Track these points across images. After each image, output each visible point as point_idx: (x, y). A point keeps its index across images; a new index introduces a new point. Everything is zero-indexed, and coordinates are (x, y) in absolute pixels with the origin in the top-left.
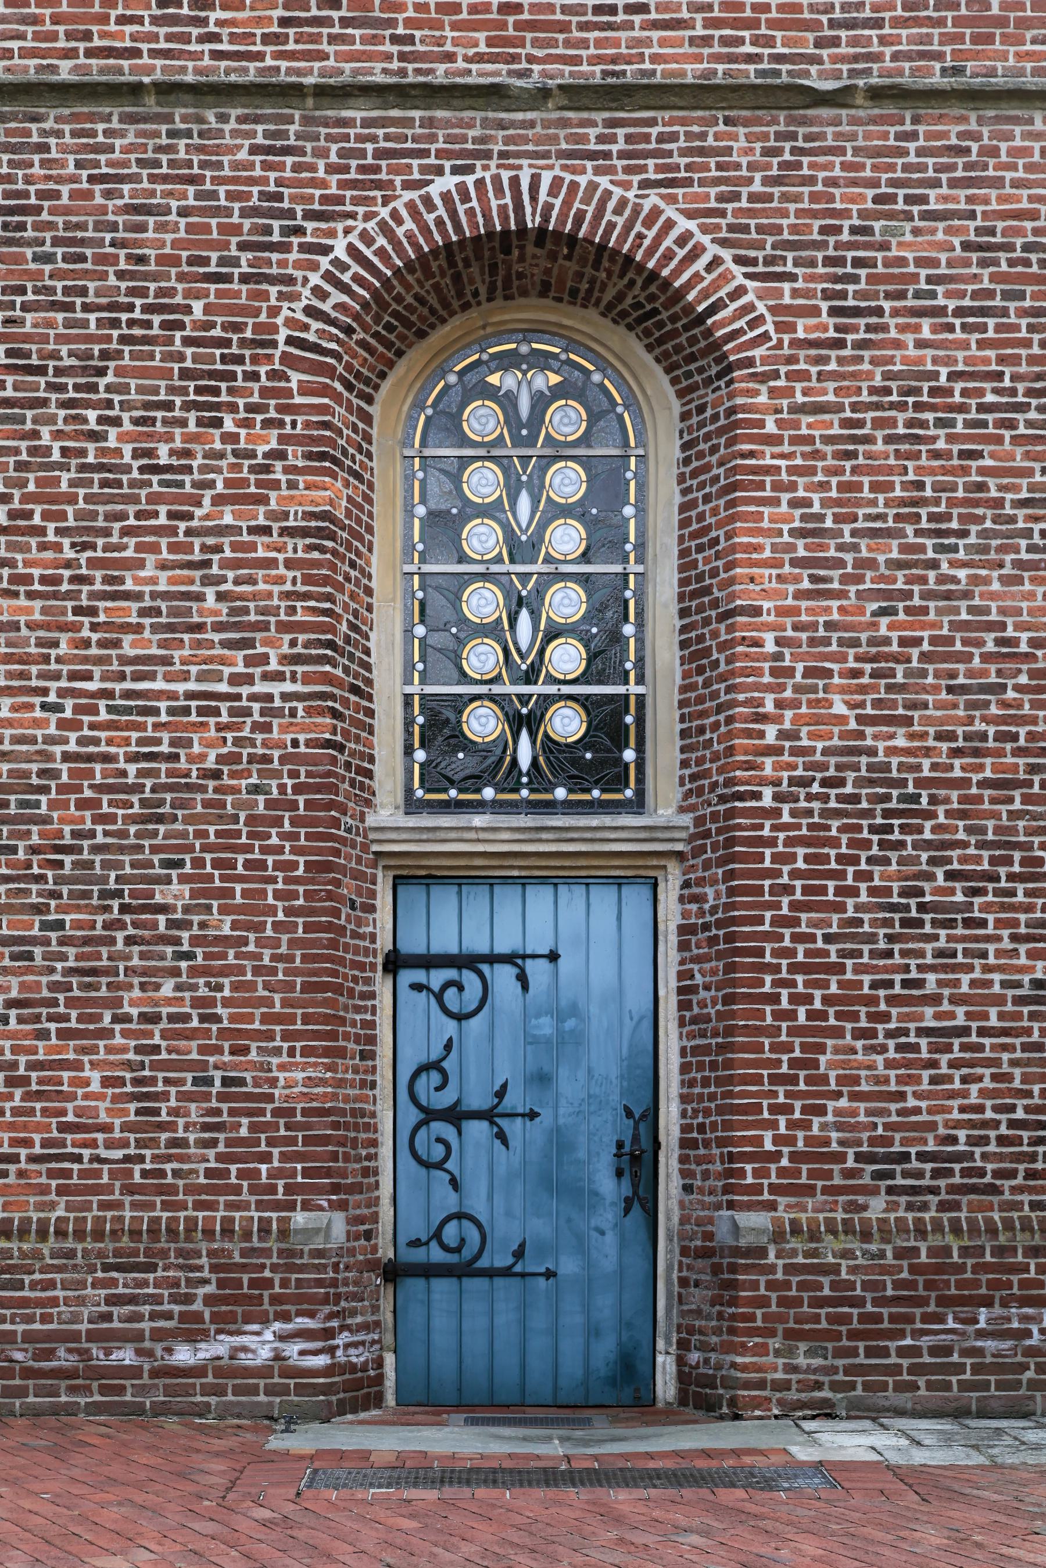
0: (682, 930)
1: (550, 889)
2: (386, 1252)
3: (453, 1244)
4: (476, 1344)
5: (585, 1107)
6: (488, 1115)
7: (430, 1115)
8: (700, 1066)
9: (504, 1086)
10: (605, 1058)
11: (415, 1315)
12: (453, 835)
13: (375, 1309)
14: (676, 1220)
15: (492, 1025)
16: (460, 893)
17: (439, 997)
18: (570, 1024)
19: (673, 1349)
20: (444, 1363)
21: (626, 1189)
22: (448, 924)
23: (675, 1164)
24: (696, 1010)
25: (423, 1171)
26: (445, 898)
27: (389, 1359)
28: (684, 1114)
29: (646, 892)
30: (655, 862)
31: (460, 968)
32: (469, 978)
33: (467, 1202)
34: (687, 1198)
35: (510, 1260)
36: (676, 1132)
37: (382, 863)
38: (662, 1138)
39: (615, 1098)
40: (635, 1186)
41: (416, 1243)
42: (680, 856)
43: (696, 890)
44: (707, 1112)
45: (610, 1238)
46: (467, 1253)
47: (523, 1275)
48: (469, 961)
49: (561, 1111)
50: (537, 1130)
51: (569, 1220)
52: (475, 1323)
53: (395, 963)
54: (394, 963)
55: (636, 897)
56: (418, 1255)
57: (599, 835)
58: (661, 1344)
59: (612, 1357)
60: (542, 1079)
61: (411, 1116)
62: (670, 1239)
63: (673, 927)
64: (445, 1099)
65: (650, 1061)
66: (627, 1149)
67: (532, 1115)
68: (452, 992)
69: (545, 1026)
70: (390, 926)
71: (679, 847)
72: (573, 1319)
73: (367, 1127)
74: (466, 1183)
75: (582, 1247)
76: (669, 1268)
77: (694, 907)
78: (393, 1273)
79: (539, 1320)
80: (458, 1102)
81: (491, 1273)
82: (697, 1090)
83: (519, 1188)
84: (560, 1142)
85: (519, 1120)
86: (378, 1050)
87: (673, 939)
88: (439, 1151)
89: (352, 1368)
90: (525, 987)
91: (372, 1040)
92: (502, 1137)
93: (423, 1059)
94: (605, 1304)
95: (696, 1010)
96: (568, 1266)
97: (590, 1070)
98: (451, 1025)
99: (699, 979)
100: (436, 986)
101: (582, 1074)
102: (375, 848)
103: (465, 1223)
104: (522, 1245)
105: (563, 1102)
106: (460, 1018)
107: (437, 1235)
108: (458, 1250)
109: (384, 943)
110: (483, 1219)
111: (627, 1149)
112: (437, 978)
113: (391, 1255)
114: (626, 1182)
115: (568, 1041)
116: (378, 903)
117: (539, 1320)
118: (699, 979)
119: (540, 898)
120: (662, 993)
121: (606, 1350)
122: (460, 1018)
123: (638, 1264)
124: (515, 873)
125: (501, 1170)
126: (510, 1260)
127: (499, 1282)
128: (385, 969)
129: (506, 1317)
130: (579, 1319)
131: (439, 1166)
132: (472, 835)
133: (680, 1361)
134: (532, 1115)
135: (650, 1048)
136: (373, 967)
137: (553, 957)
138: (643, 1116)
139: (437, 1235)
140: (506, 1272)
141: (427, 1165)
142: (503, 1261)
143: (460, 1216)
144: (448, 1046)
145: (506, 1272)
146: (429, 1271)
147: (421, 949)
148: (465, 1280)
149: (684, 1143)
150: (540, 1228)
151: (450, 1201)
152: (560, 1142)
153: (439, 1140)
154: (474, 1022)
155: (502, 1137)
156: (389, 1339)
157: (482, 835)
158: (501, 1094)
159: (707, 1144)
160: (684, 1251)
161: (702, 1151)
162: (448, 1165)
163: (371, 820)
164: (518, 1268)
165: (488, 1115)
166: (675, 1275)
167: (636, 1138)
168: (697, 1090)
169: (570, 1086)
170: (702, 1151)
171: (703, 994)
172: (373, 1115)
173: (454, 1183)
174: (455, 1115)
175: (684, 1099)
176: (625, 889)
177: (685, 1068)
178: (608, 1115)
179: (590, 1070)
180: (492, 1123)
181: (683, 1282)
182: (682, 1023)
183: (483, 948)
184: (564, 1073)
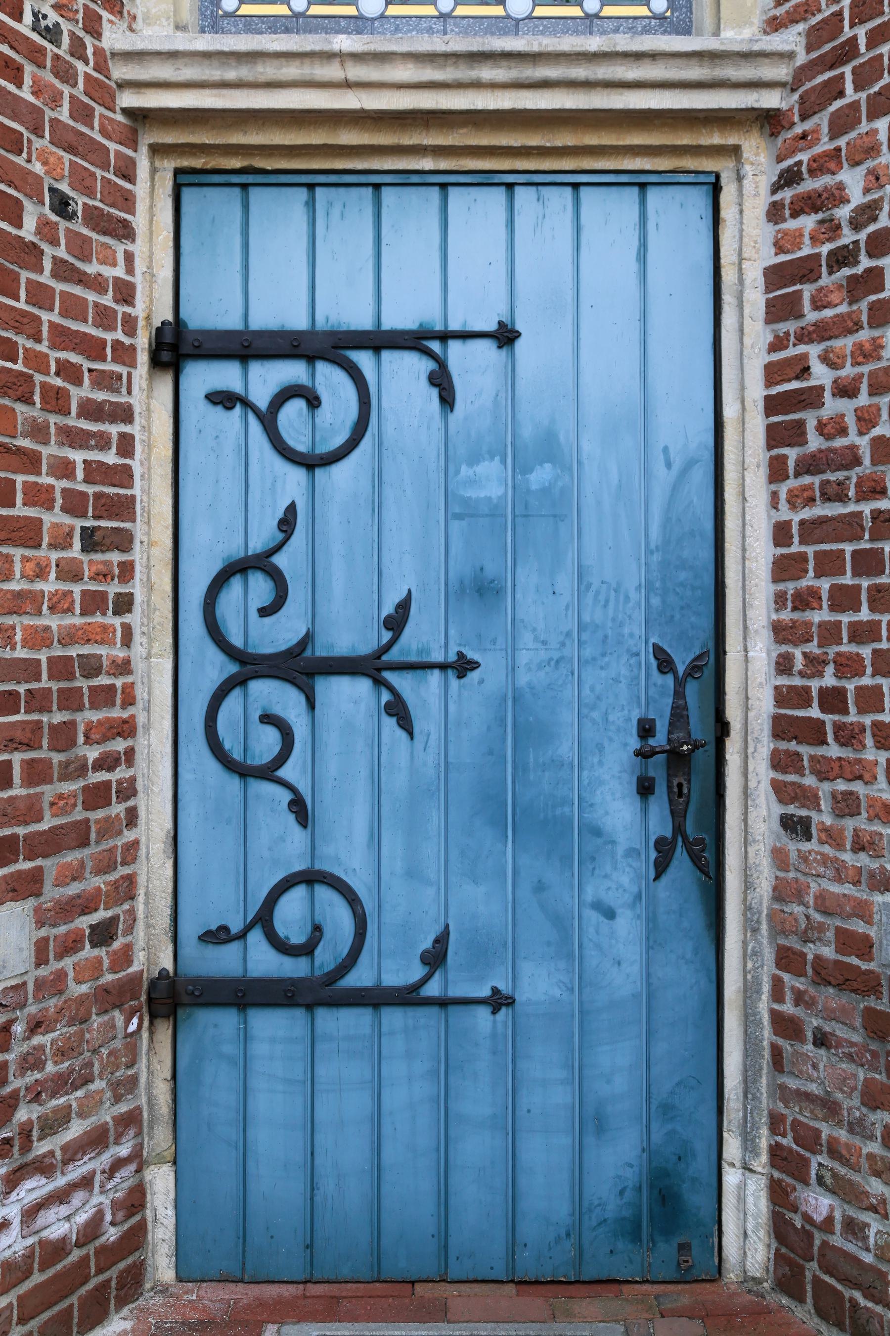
0: (775, 276)
1: (500, 194)
2: (151, 951)
3: (297, 938)
4: (344, 1151)
5: (571, 650)
6: (370, 667)
7: (248, 666)
8: (829, 564)
9: (404, 606)
10: (614, 548)
11: (218, 1086)
12: (292, 71)
13: (124, 1087)
14: (764, 887)
15: (378, 479)
16: (311, 204)
17: (268, 421)
18: (541, 476)
19: (761, 1162)
20: (276, 1185)
21: (660, 822)
22: (285, 265)
23: (762, 772)
24: (814, 442)
25: (234, 783)
26: (280, 217)
27: (161, 1182)
28: (783, 665)
29: (696, 201)
30: (716, 139)
31: (311, 359)
32: (331, 380)
33: (327, 850)
34: (794, 847)
35: (417, 972)
36: (764, 705)
37: (147, 138)
38: (733, 713)
39: (636, 634)
40: (678, 816)
41: (218, 936)
42: (770, 121)
43: (810, 185)
44: (848, 666)
45: (627, 925)
46: (326, 957)
47: (443, 1003)
48: (330, 346)
49: (523, 657)
50: (473, 697)
51: (540, 887)
52: (344, 1104)
53: (175, 349)
54: (175, 349)
55: (676, 214)
56: (224, 962)
57: (603, 72)
58: (732, 1147)
59: (630, 1176)
60: (482, 591)
61: (213, 668)
62: (750, 926)
63: (754, 274)
64: (279, 634)
65: (707, 554)
66: (660, 739)
67: (463, 666)
68: (295, 408)
69: (489, 481)
70: (166, 273)
71: (771, 100)
72: (548, 1095)
73: (104, 697)
74: (325, 809)
75: (566, 944)
76: (750, 991)
77: (808, 222)
78: (169, 999)
79: (477, 1099)
80: (307, 640)
81: (376, 999)
82: (819, 616)
83: (435, 821)
84: (521, 724)
85: (435, 676)
86: (139, 529)
87: (756, 298)
88: (268, 742)
89: (54, 1251)
90: (447, 400)
91: (124, 508)
92: (399, 711)
93: (233, 547)
94: (617, 1066)
95: (814, 442)
96: (539, 984)
97: (581, 573)
98: (292, 482)
99: (821, 375)
100: (261, 398)
101: (565, 582)
102: (128, 100)
103: (323, 893)
104: (442, 940)
105: (526, 638)
106: (311, 463)
107: (264, 918)
108: (307, 950)
109: (153, 305)
110: (359, 884)
111: (660, 739)
112: (265, 380)
113: (166, 962)
114: (659, 806)
115: (535, 514)
116: (139, 221)
117: (477, 1099)
118: (821, 375)
119: (477, 215)
120: (730, 411)
121: (618, 1161)
122: (311, 463)
123: (681, 976)
124: (427, 164)
125: (397, 782)
126: (417, 972)
127: (394, 1018)
128: (156, 363)
129: (407, 1091)
130: (561, 1096)
131: (268, 772)
132: (332, 72)
133: (779, 1195)
134: (463, 666)
135: (709, 525)
136: (124, 353)
137: (505, 336)
138: (694, 669)
139: (264, 918)
140: (408, 997)
141: (243, 771)
142: (401, 972)
143: (310, 878)
144: (287, 523)
145: (408, 997)
146: (246, 995)
147: (231, 321)
148: (322, 1013)
149: (781, 728)
150: (477, 904)
151: (291, 848)
152: (521, 724)
153: (268, 719)
154: (341, 472)
155: (399, 711)
156: (160, 1138)
157: (356, 72)
158: (397, 622)
159: (848, 736)
160: (787, 960)
161: (833, 750)
162: (286, 772)
163: (114, 37)
164: (433, 989)
165: (370, 667)
166: (764, 1005)
167: (679, 716)
168: (819, 616)
169: (540, 605)
170: (833, 750)
171: (832, 406)
172: (124, 667)
173: (300, 809)
174: (302, 667)
175: (781, 633)
176: (653, 195)
177: (785, 568)
178: (620, 667)
179: (581, 573)
180: (379, 683)
181: (785, 1026)
182: (777, 471)
183: (360, 319)
184: (528, 577)
